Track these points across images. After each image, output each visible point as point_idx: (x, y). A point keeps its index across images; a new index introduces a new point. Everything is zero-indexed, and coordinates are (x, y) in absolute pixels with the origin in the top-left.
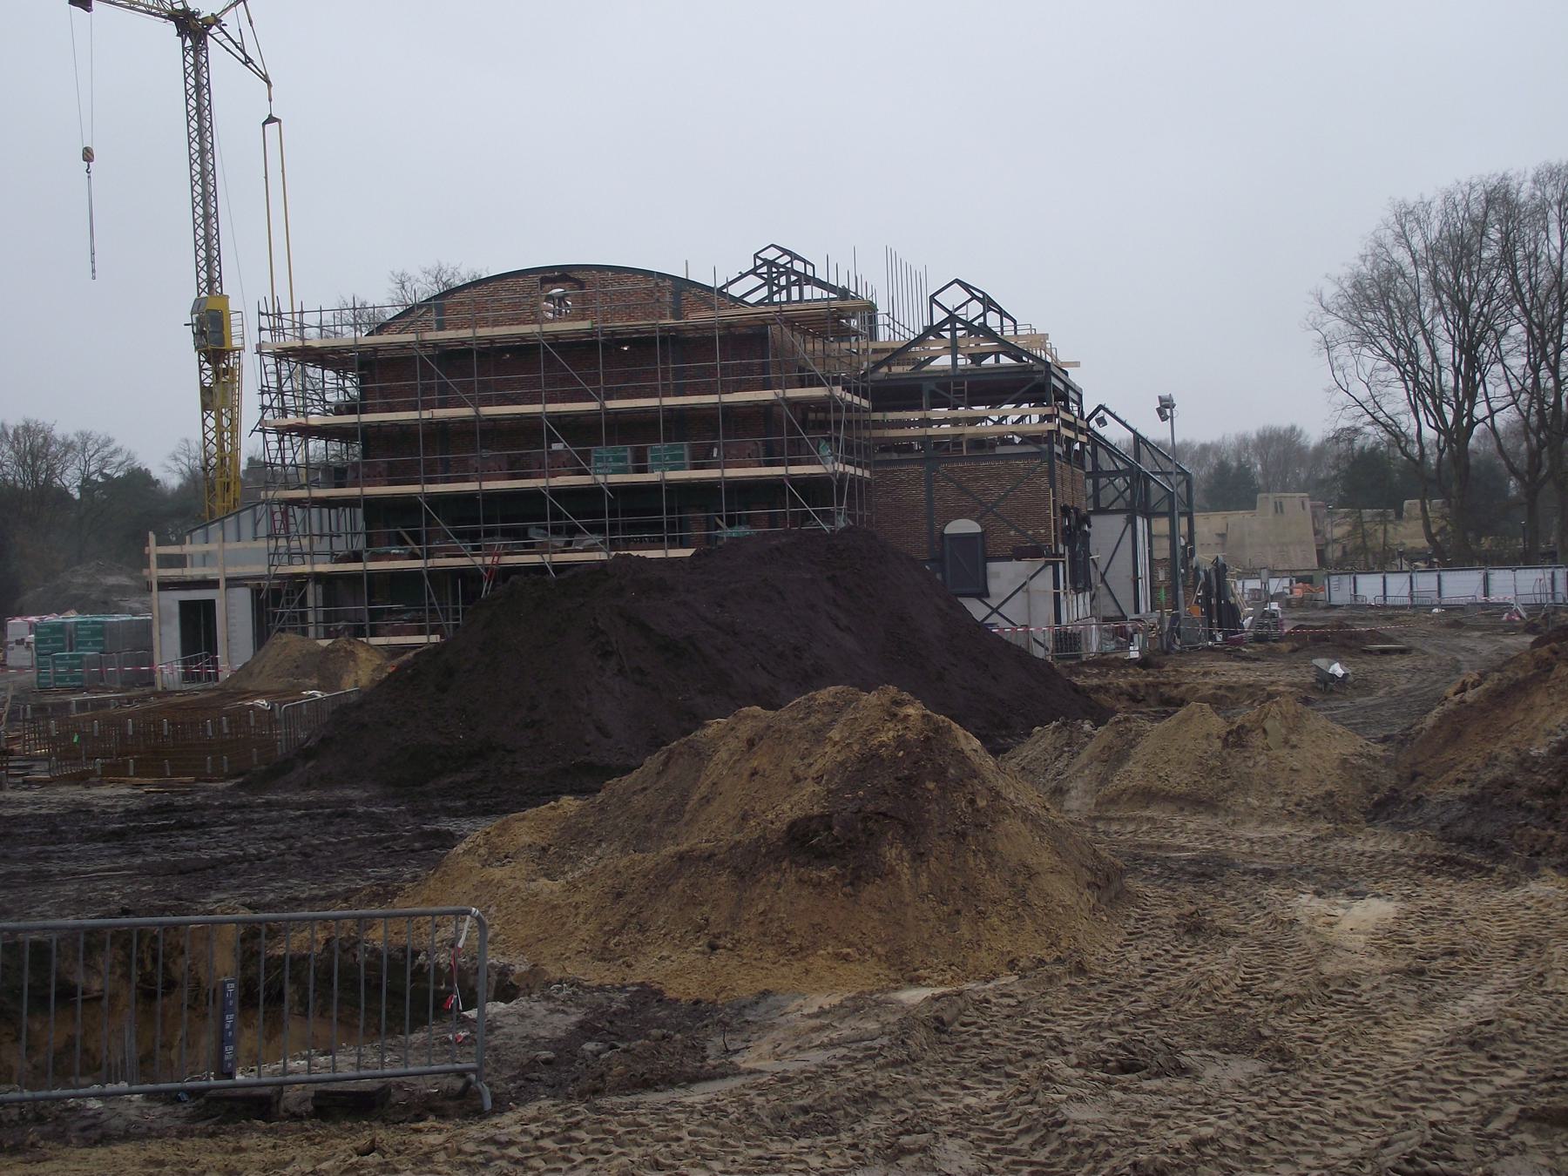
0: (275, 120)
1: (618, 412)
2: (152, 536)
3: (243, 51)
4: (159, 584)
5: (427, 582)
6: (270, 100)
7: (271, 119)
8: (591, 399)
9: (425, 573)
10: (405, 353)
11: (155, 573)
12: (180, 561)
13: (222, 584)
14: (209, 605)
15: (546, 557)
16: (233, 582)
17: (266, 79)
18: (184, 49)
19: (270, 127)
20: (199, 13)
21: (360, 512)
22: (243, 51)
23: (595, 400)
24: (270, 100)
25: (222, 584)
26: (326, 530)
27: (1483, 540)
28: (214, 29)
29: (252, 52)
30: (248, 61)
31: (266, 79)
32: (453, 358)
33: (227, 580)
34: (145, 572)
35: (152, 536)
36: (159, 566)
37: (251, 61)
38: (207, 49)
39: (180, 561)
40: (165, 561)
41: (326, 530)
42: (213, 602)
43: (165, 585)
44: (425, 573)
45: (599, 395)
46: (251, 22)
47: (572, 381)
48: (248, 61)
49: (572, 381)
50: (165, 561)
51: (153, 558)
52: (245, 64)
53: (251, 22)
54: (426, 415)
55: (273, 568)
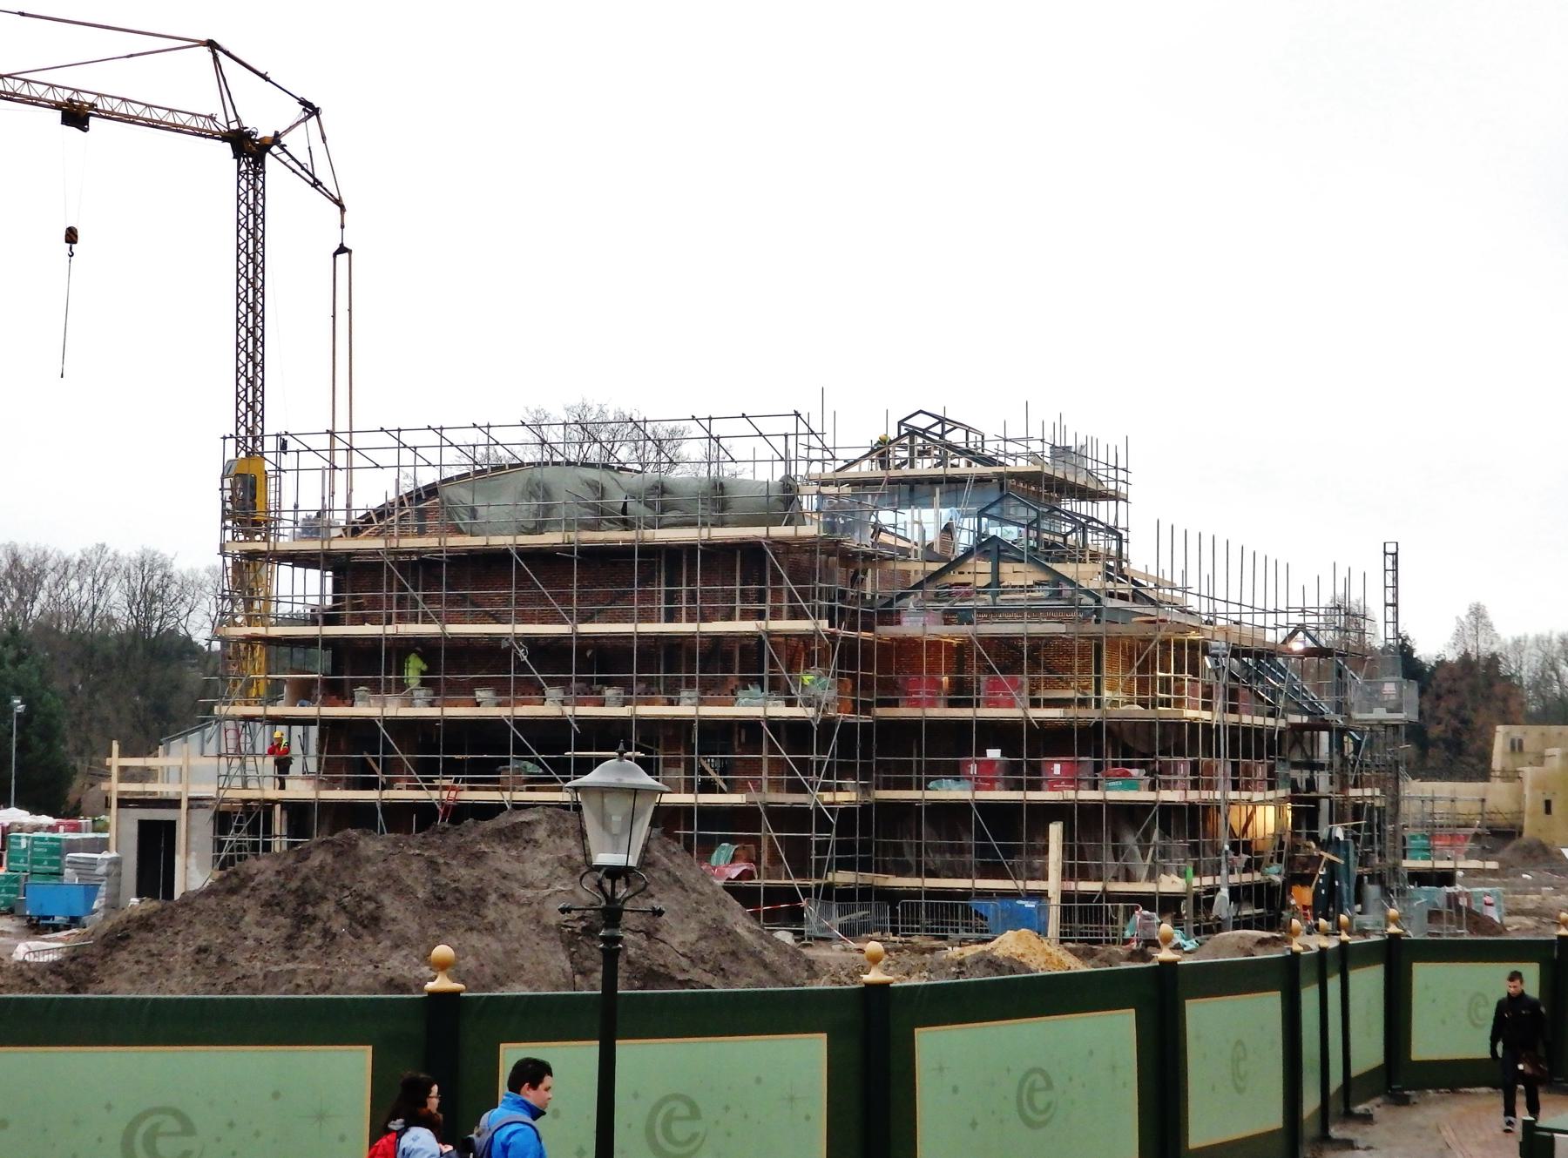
0: (349, 251)
1: (596, 638)
2: (115, 746)
3: (312, 176)
4: (119, 801)
5: (380, 816)
6: (342, 227)
7: (342, 249)
8: (563, 622)
9: (378, 805)
10: (371, 559)
11: (116, 787)
12: (146, 775)
13: (184, 805)
14: (171, 826)
15: (507, 795)
16: (195, 802)
17: (338, 202)
18: (239, 173)
19: (343, 258)
20: (256, 134)
21: (314, 731)
22: (312, 176)
23: (566, 623)
24: (342, 227)
25: (184, 805)
26: (224, 751)
27: (448, 841)
28: (275, 149)
29: (323, 174)
30: (316, 184)
31: (338, 202)
32: (423, 569)
33: (190, 799)
34: (104, 786)
35: (115, 746)
36: (121, 780)
37: (320, 184)
38: (264, 172)
39: (146, 775)
40: (127, 775)
41: (224, 751)
42: (173, 823)
43: (123, 803)
44: (378, 805)
45: (572, 619)
46: (324, 138)
47: (542, 599)
48: (316, 184)
49: (542, 599)
50: (127, 775)
51: (115, 771)
52: (314, 185)
53: (324, 138)
54: (390, 629)
55: (222, 791)
